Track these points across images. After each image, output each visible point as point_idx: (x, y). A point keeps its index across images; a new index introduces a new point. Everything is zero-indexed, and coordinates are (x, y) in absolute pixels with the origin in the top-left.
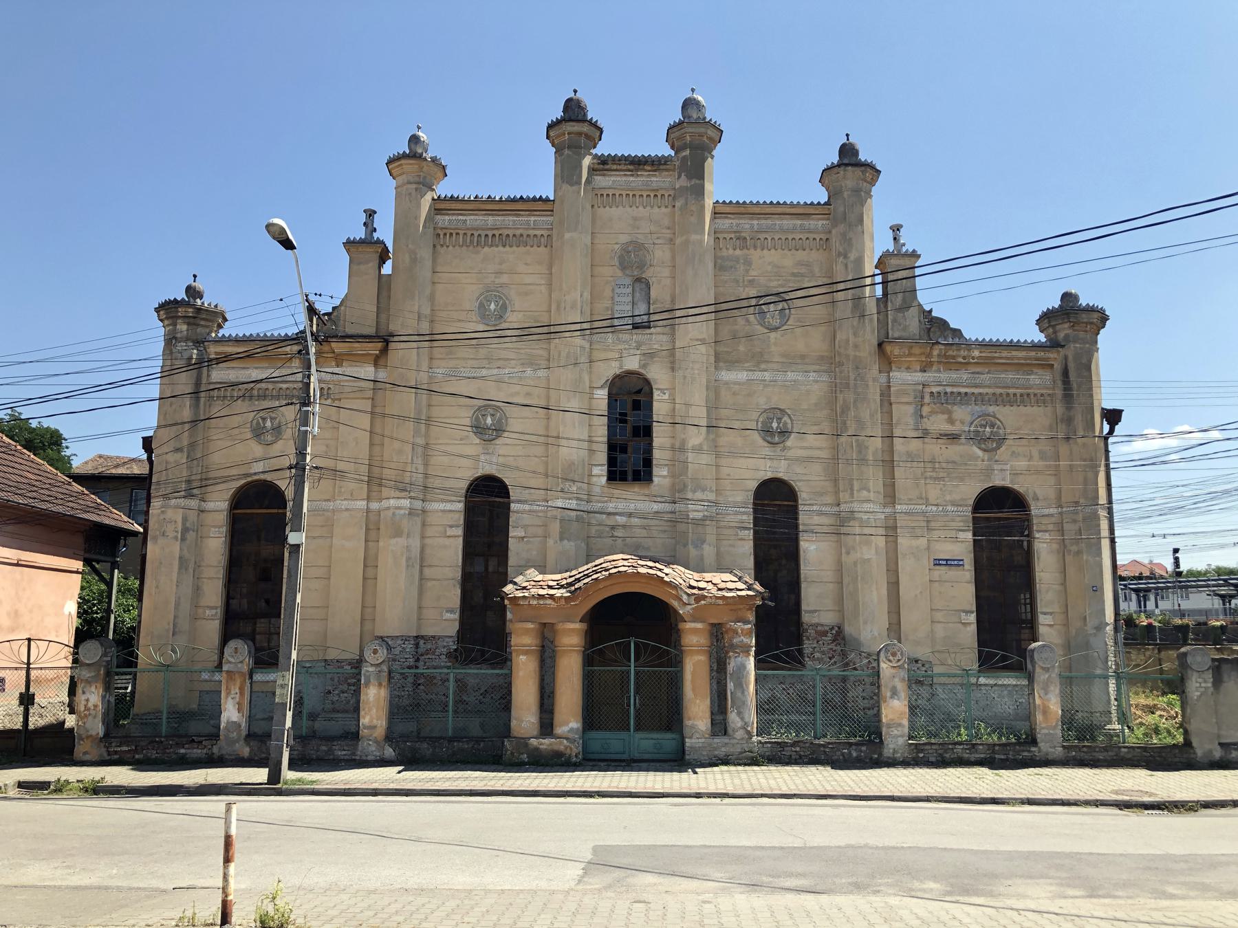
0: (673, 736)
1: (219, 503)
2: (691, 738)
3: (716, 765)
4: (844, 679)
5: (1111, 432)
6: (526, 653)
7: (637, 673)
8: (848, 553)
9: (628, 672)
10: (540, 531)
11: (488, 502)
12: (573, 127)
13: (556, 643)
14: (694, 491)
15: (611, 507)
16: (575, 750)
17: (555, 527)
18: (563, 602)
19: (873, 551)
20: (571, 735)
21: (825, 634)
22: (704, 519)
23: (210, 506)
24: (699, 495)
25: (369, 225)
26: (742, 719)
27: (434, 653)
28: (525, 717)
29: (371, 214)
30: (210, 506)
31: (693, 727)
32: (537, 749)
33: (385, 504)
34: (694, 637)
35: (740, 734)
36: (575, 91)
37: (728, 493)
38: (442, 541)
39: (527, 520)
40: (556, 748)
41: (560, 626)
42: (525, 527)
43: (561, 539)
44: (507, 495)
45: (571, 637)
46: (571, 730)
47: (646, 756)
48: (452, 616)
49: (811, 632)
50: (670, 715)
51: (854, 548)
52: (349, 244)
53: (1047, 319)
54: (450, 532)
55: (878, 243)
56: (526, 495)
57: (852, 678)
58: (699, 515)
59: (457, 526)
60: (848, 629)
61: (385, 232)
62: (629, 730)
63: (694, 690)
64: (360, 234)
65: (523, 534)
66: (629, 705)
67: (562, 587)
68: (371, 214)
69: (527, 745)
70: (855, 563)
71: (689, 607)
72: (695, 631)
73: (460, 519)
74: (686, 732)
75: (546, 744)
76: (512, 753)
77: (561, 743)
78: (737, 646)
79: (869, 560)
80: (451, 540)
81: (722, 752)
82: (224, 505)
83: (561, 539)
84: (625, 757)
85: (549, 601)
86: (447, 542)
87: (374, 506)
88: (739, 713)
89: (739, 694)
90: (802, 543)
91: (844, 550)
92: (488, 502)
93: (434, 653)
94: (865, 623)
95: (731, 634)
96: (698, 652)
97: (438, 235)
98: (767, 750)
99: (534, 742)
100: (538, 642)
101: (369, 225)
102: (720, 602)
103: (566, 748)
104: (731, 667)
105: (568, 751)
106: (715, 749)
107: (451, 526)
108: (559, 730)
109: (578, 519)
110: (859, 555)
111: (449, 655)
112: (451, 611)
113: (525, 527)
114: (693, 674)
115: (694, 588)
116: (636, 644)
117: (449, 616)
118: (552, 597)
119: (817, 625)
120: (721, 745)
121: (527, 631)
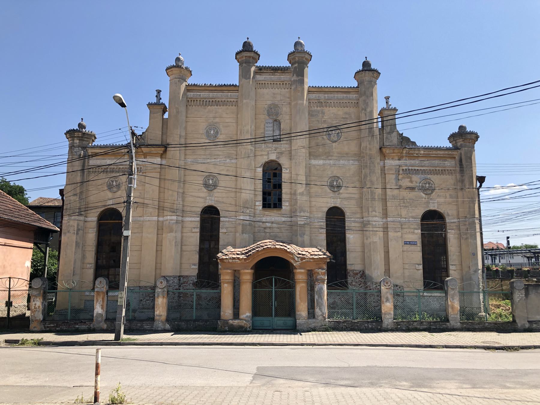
1: (93, 218)
4: (365, 294)
5: (480, 186)
6: (227, 283)
7: (275, 292)
8: (367, 239)
9: (272, 291)
10: (233, 230)
11: (210, 217)
12: (247, 54)
14: (300, 212)
15: (264, 219)
16: (248, 325)
17: (240, 228)
19: (378, 238)
20: (247, 319)
21: (357, 274)
23: (89, 219)
24: (302, 214)
25: (158, 97)
26: (321, 311)
28: (227, 311)
29: (159, 92)
30: (89, 219)
31: (300, 315)
32: (232, 325)
33: (165, 218)
34: (300, 276)
35: (320, 318)
36: (248, 38)
37: (315, 213)
39: (227, 225)
40: (240, 324)
41: (242, 271)
42: (227, 228)
43: (243, 233)
44: (344, 216)
45: (247, 276)
46: (247, 316)
47: (280, 328)
50: (290, 310)
52: (150, 105)
53: (453, 137)
55: (379, 104)
56: (227, 214)
57: (369, 294)
58: (302, 223)
60: (367, 272)
61: (165, 100)
62: (272, 316)
63: (300, 298)
64: (154, 100)
67: (243, 254)
68: (159, 92)
69: (227, 323)
70: (370, 243)
72: (301, 273)
74: (297, 317)
75: (236, 322)
76: (221, 327)
77: (243, 322)
78: (319, 280)
79: (376, 242)
81: (312, 326)
82: (95, 219)
83: (243, 233)
85: (237, 260)
86: (192, 234)
87: (161, 219)
88: (320, 309)
89: (320, 301)
90: (347, 235)
92: (210, 217)
94: (374, 269)
95: (316, 274)
97: (188, 101)
99: (231, 322)
100: (232, 278)
101: (158, 97)
102: (312, 260)
105: (246, 326)
107: (194, 228)
108: (242, 316)
112: (194, 265)
113: (227, 228)
115: (300, 254)
117: (193, 267)
118: (238, 258)
119: (353, 270)
120: (312, 323)
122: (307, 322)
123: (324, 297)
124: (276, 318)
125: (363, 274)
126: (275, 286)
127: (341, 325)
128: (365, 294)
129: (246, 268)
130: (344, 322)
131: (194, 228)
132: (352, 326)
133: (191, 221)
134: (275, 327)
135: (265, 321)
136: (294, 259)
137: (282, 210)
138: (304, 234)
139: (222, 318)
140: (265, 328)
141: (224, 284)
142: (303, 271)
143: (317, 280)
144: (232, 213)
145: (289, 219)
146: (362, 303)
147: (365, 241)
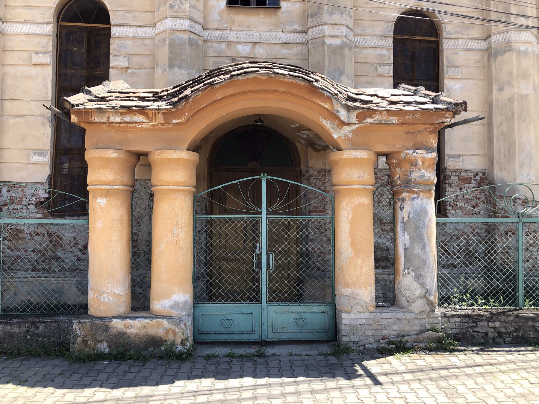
0: (322, 308)
2: (349, 312)
3: (391, 353)
4: (490, 229)
6: (107, 194)
7: (270, 222)
8: (501, 89)
9: (257, 224)
10: (147, 62)
13: (154, 181)
14: (331, 13)
15: (231, 36)
16: (179, 334)
17: (164, 53)
18: (160, 119)
19: (531, 87)
20: (174, 313)
21: (468, 180)
22: (342, 47)
24: (337, 18)
26: (423, 285)
27: (20, 203)
28: (107, 286)
31: (352, 297)
32: (122, 334)
35: (419, 305)
37: (366, 23)
38: (26, 70)
39: (130, 46)
40: (152, 332)
41: (156, 156)
42: (129, 56)
43: (171, 66)
44: (108, 22)
45: (176, 176)
46: (175, 305)
47: (285, 337)
48: (41, 159)
49: (454, 178)
50: (308, 273)
51: (509, 83)
54: (36, 59)
56: (129, 19)
57: (502, 228)
58: (337, 42)
59: (45, 53)
60: (498, 174)
62: (259, 301)
63: (353, 244)
65: (126, 64)
66: (260, 267)
67: (161, 98)
69: (107, 329)
70: (511, 100)
71: (347, 130)
72: (356, 162)
73: (49, 44)
74: (341, 303)
75: (137, 327)
76: (84, 341)
77: (159, 325)
78: (416, 184)
79: (526, 96)
80: (38, 68)
81: (392, 331)
83: (171, 66)
84: (254, 338)
85: (139, 118)
86: (33, 71)
88: (418, 278)
89: (417, 250)
90: (446, 81)
91: (495, 87)
93: (20, 203)
94: (522, 166)
95: (406, 167)
96: (359, 192)
98: (453, 327)
99: (118, 325)
100: (126, 178)
102: (394, 120)
103: (167, 331)
104: (403, 215)
105: (170, 337)
106: (384, 327)
107: (37, 53)
108: (159, 304)
109: (191, 42)
110: (516, 90)
111: (40, 204)
112: (40, 153)
113: (129, 56)
114: (353, 222)
115: (355, 100)
116: (268, 182)
117: (36, 159)
118: (142, 110)
119: (460, 171)
120: (392, 323)
121: (107, 162)
122: (377, 322)
123: (429, 239)
124: (274, 308)
125: (485, 180)
126: (269, 205)
127: (483, 327)
128: (490, 229)
129: (171, 145)
130: (492, 317)
131: (37, 53)
132: (517, 330)
133: (27, 35)
134: (271, 336)
135: (235, 317)
136: (334, 116)
137: (280, 13)
138: (342, 73)
139: (92, 310)
140: (237, 338)
141: (95, 197)
142: (362, 154)
143: (408, 184)
144: (143, 15)
145: (299, 38)
146: (481, 249)
147: (495, 95)
